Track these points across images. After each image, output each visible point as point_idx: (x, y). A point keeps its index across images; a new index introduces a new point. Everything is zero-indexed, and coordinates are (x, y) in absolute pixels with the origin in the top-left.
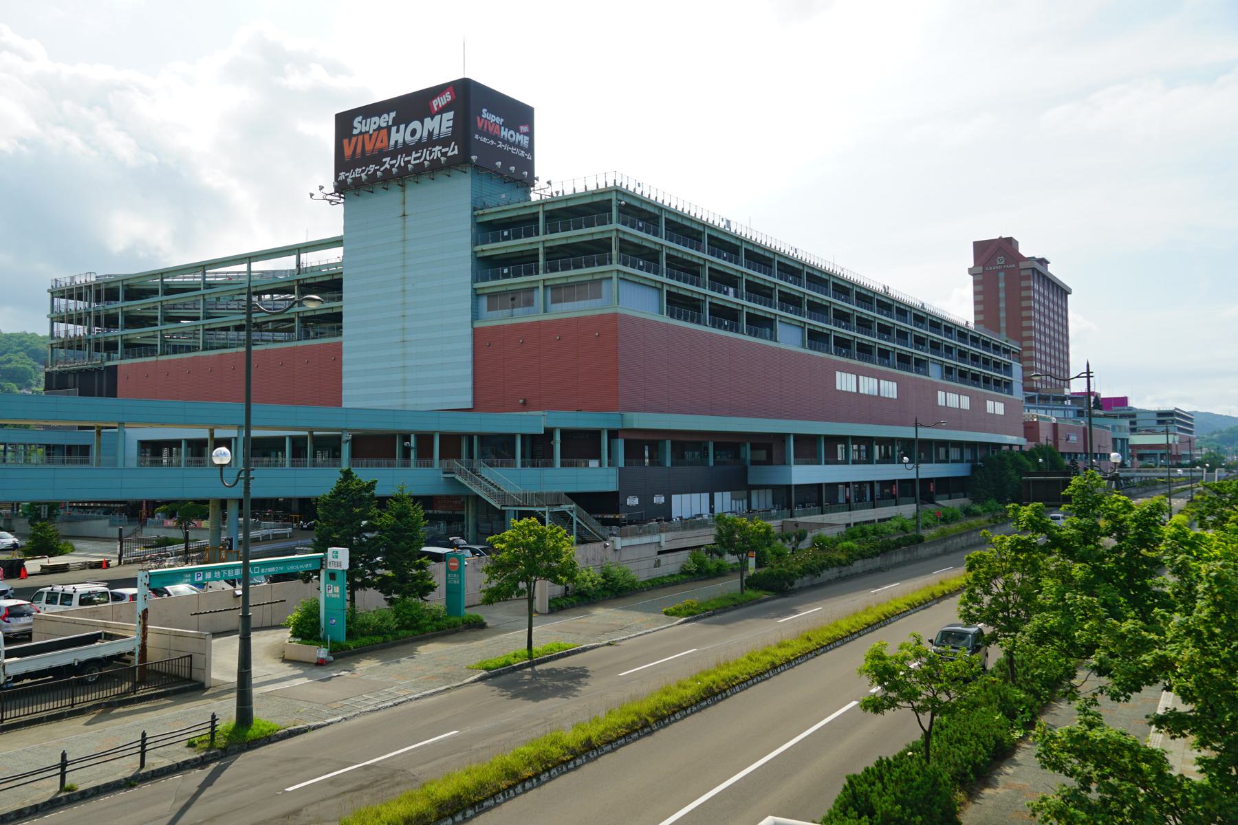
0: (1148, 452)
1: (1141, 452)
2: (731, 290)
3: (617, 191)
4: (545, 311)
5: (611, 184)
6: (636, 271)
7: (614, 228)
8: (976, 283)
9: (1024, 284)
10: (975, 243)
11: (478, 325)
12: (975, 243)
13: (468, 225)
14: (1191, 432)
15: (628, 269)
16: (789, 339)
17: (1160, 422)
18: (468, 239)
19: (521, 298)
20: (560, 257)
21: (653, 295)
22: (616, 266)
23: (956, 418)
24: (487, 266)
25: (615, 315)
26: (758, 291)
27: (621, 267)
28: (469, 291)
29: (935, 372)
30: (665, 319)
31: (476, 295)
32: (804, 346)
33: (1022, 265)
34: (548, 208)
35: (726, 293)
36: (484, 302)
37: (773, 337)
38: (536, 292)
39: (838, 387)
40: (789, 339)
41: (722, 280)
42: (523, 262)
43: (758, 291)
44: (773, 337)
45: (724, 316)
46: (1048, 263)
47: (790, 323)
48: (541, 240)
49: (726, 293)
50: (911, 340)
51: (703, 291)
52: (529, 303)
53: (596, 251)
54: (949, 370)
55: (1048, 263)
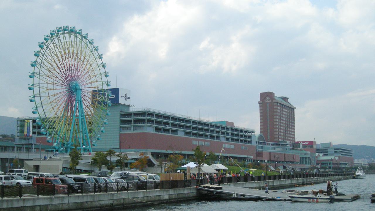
0: (325, 162)
1: (323, 162)
2: (168, 126)
3: (147, 111)
4: (133, 131)
5: (145, 110)
6: (149, 125)
7: (146, 117)
8: (260, 106)
9: (275, 107)
10: (261, 93)
11: (121, 133)
12: (261, 93)
13: (119, 115)
14: (352, 156)
15: (148, 124)
16: (181, 134)
17: (335, 152)
18: (119, 117)
19: (127, 128)
20: (136, 121)
21: (152, 128)
22: (146, 124)
23: (308, 150)
24: (123, 122)
25: (146, 132)
26: (173, 125)
27: (147, 124)
28: (119, 127)
29: (223, 140)
30: (155, 132)
31: (120, 127)
32: (184, 136)
33: (274, 101)
34: (134, 113)
35: (167, 126)
36: (122, 129)
37: (177, 134)
38: (132, 128)
39: (193, 144)
40: (181, 134)
41: (166, 124)
42: (130, 122)
43: (173, 125)
44: (177, 134)
45: (166, 130)
46: (288, 98)
47: (181, 131)
48: (133, 118)
49: (167, 126)
50: (215, 132)
51: (163, 127)
52: (130, 129)
53: (143, 121)
54: (227, 139)
55: (288, 98)
